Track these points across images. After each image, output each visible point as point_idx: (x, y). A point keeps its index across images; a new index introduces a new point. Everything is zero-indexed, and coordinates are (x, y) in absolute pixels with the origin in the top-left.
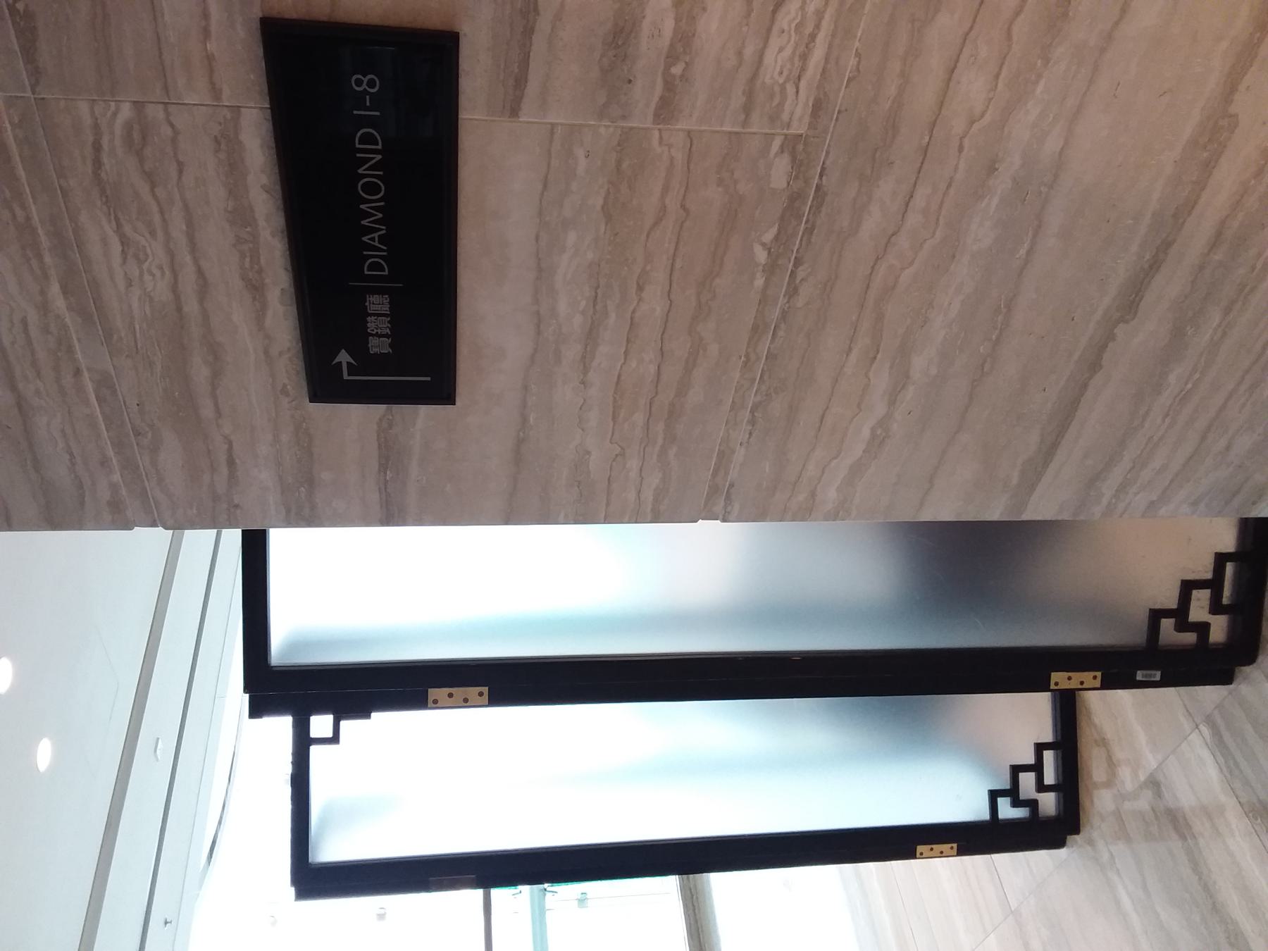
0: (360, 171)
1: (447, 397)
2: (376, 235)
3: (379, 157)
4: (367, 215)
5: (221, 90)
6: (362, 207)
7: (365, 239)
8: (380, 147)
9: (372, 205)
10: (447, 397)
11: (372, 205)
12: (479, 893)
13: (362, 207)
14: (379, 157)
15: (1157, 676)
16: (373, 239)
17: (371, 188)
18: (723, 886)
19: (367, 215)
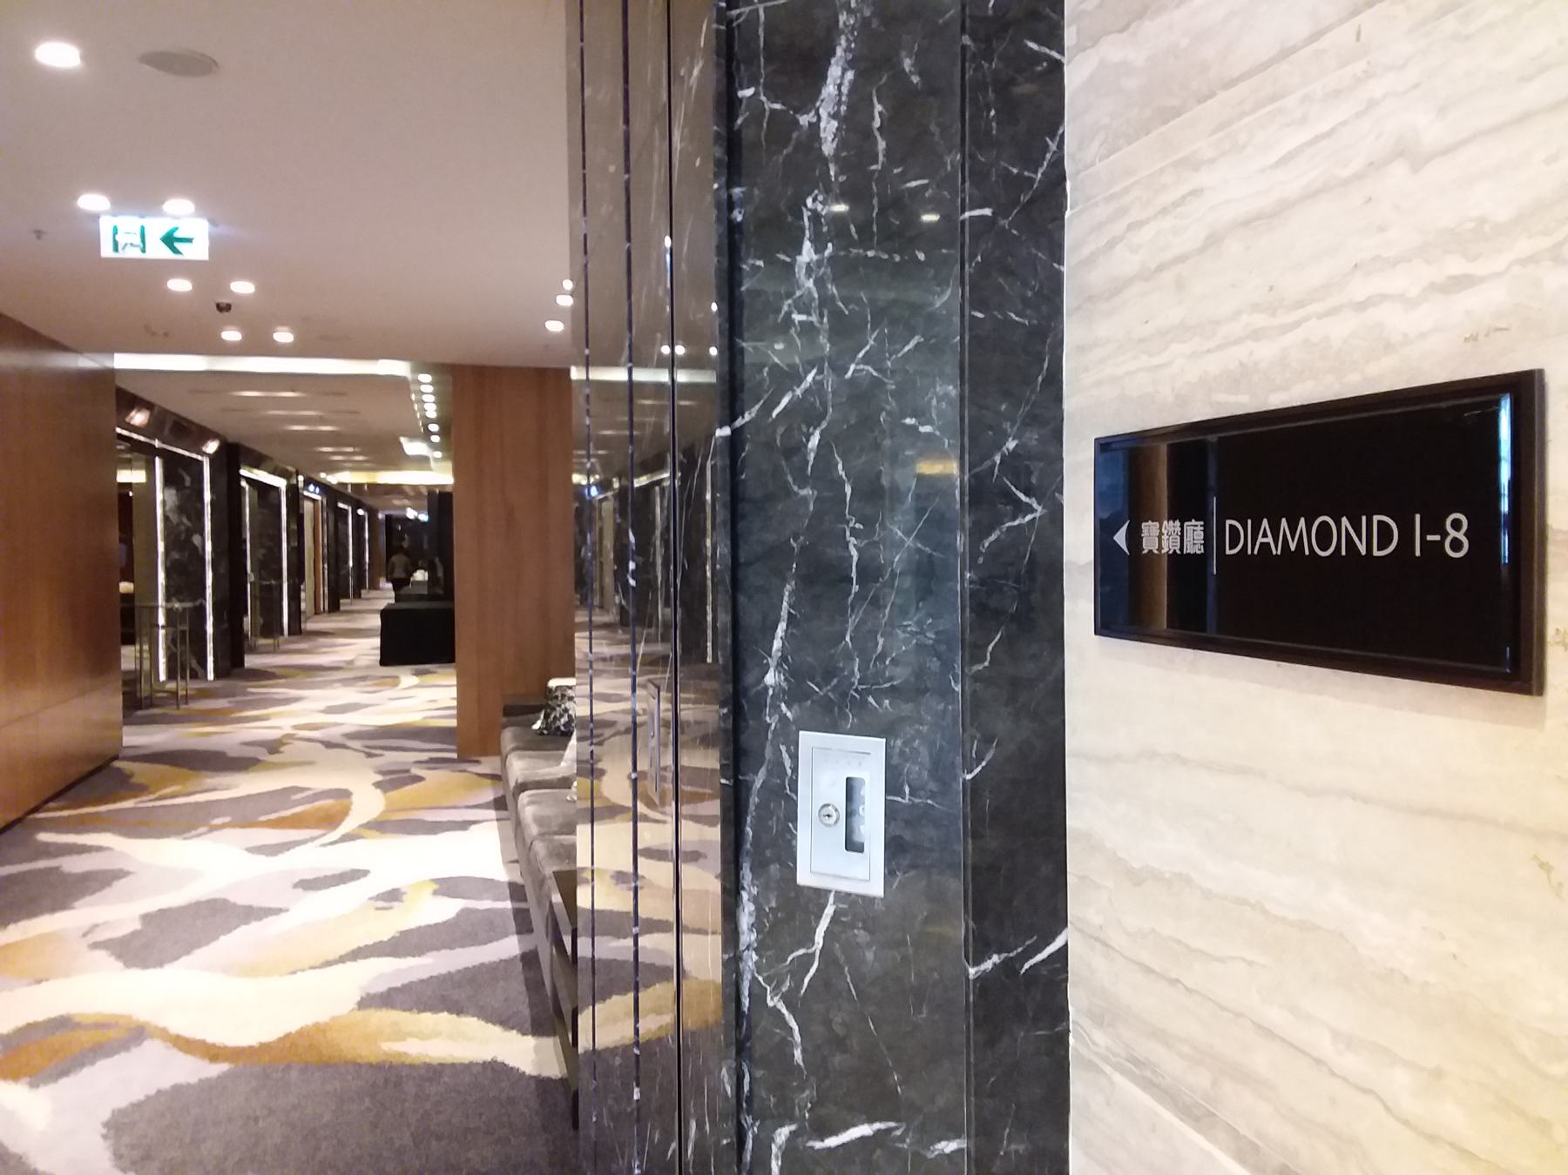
0: (1344, 520)
1: (1525, 390)
2: (1270, 539)
3: (1363, 552)
4: (1293, 527)
5: (1451, 278)
6: (1302, 521)
7: (1265, 523)
8: (1376, 553)
9: (1299, 535)
10: (1525, 390)
11: (1299, 535)
12: (599, 1045)
13: (1302, 521)
14: (1363, 552)
15: (227, 819)
16: (1265, 535)
17: (1324, 536)
18: (630, 737)
19: (1293, 527)
